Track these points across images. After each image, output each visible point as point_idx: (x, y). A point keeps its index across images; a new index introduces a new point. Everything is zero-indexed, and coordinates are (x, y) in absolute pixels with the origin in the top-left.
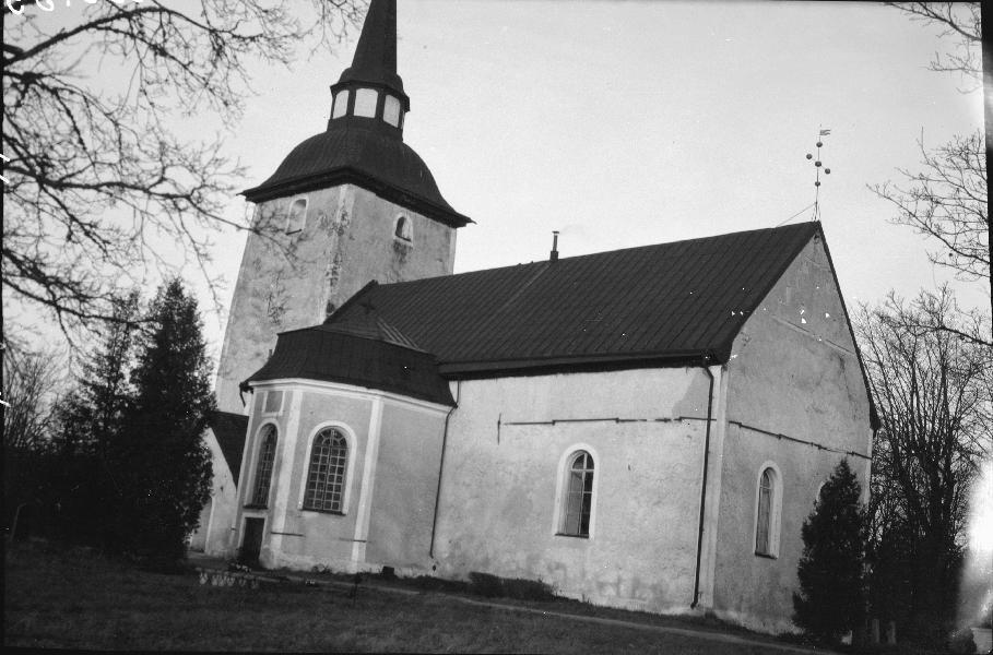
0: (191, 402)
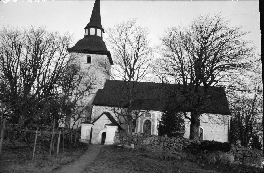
0: (174, 128)
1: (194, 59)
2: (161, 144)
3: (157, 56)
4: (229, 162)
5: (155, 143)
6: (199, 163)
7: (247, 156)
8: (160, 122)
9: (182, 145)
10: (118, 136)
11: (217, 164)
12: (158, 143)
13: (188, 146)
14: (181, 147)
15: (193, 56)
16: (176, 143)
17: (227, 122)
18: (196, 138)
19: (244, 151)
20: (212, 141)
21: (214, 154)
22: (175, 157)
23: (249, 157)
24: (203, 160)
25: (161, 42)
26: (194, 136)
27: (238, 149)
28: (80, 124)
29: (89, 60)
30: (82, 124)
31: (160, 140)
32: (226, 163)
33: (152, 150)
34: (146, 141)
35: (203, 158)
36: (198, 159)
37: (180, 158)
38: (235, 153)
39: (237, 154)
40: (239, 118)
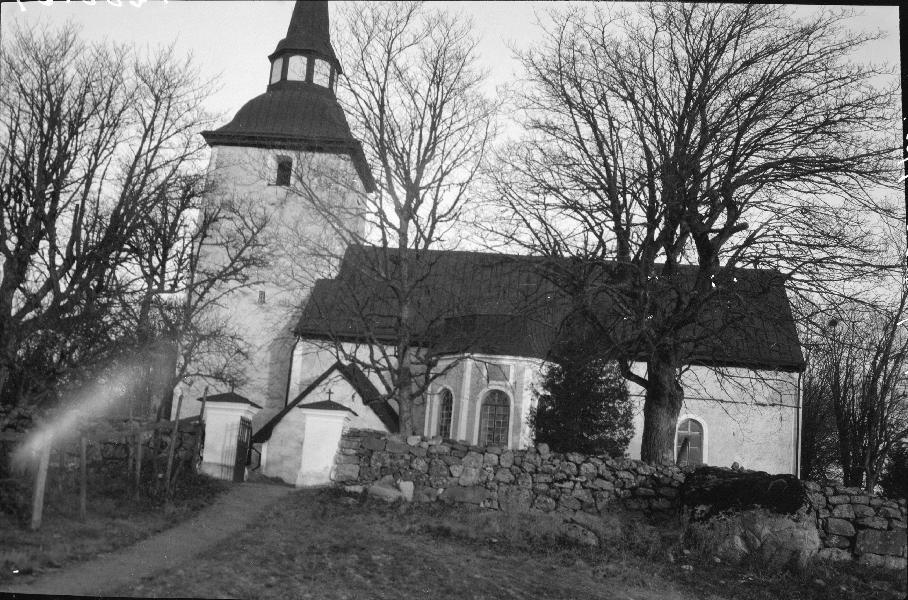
1: (662, 147)
2: (523, 482)
3: (511, 130)
4: (796, 553)
5: (500, 476)
6: (672, 559)
7: (872, 528)
8: (543, 399)
9: (607, 485)
10: (353, 452)
11: (745, 562)
12: (512, 477)
13: (633, 489)
14: (606, 495)
15: (657, 130)
16: (584, 479)
17: (792, 392)
18: (665, 455)
19: (858, 509)
20: (730, 467)
21: (738, 520)
22: (573, 534)
23: (881, 529)
24: (689, 548)
25: (520, 69)
26: (660, 451)
27: (834, 500)
28: (200, 403)
29: (284, 171)
30: (208, 404)
31: (520, 467)
32: (785, 557)
33: (488, 505)
34: (465, 471)
35: (692, 539)
36: (667, 541)
37: (593, 542)
38: (821, 516)
39: (830, 520)
40: (836, 386)
